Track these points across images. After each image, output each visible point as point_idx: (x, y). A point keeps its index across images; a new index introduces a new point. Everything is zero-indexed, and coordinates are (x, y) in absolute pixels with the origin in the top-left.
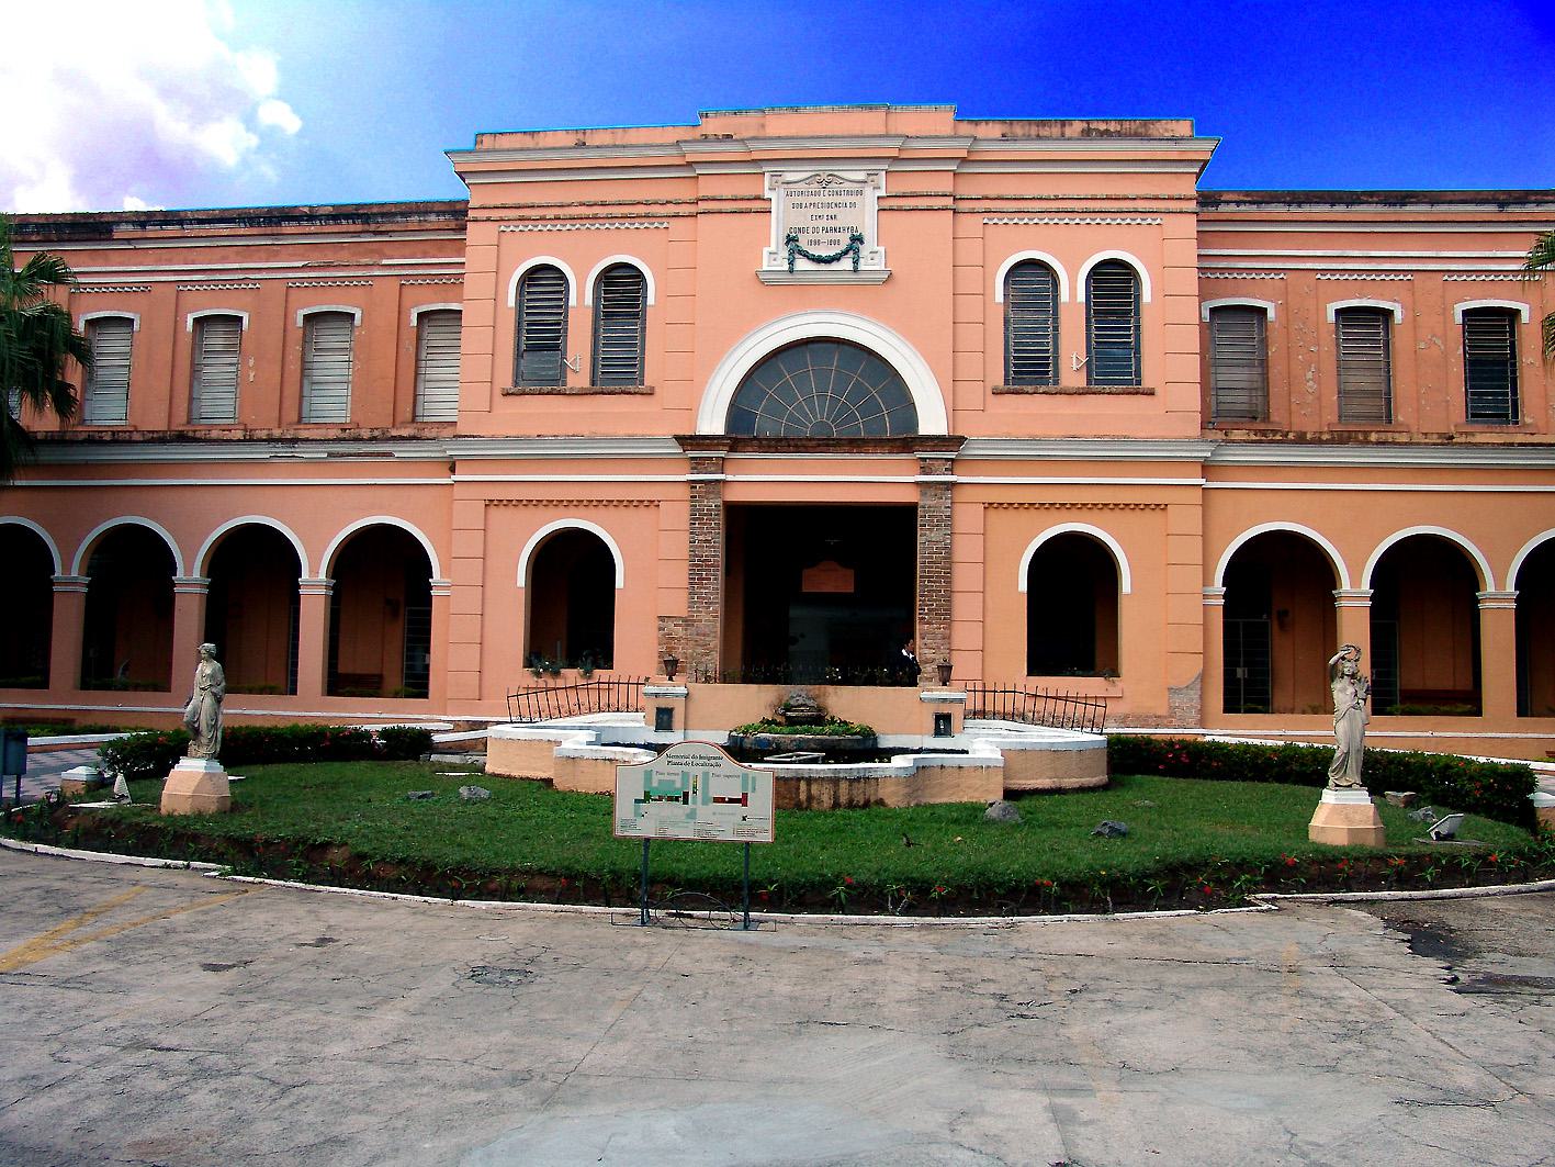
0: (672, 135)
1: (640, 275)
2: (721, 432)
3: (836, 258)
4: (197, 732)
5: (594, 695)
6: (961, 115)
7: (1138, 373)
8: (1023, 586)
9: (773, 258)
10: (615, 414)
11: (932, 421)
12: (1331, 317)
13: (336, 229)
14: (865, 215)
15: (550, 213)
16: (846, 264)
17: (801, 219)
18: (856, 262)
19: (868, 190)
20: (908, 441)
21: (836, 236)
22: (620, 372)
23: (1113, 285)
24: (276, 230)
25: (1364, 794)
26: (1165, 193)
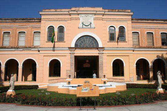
0: (67, 10)
1: (124, 27)
2: (74, 47)
3: (88, 26)
4: (11, 86)
5: (60, 80)
6: (103, 9)
7: (125, 40)
8: (112, 66)
9: (81, 25)
10: (121, 44)
11: (100, 45)
12: (160, 34)
13: (23, 21)
14: (92, 21)
15: (52, 19)
16: (90, 26)
17: (84, 21)
18: (91, 26)
19: (92, 17)
20: (97, 48)
21: (88, 23)
22: (61, 39)
23: (122, 29)
24: (15, 21)
25: (162, 89)
26: (120, 18)
